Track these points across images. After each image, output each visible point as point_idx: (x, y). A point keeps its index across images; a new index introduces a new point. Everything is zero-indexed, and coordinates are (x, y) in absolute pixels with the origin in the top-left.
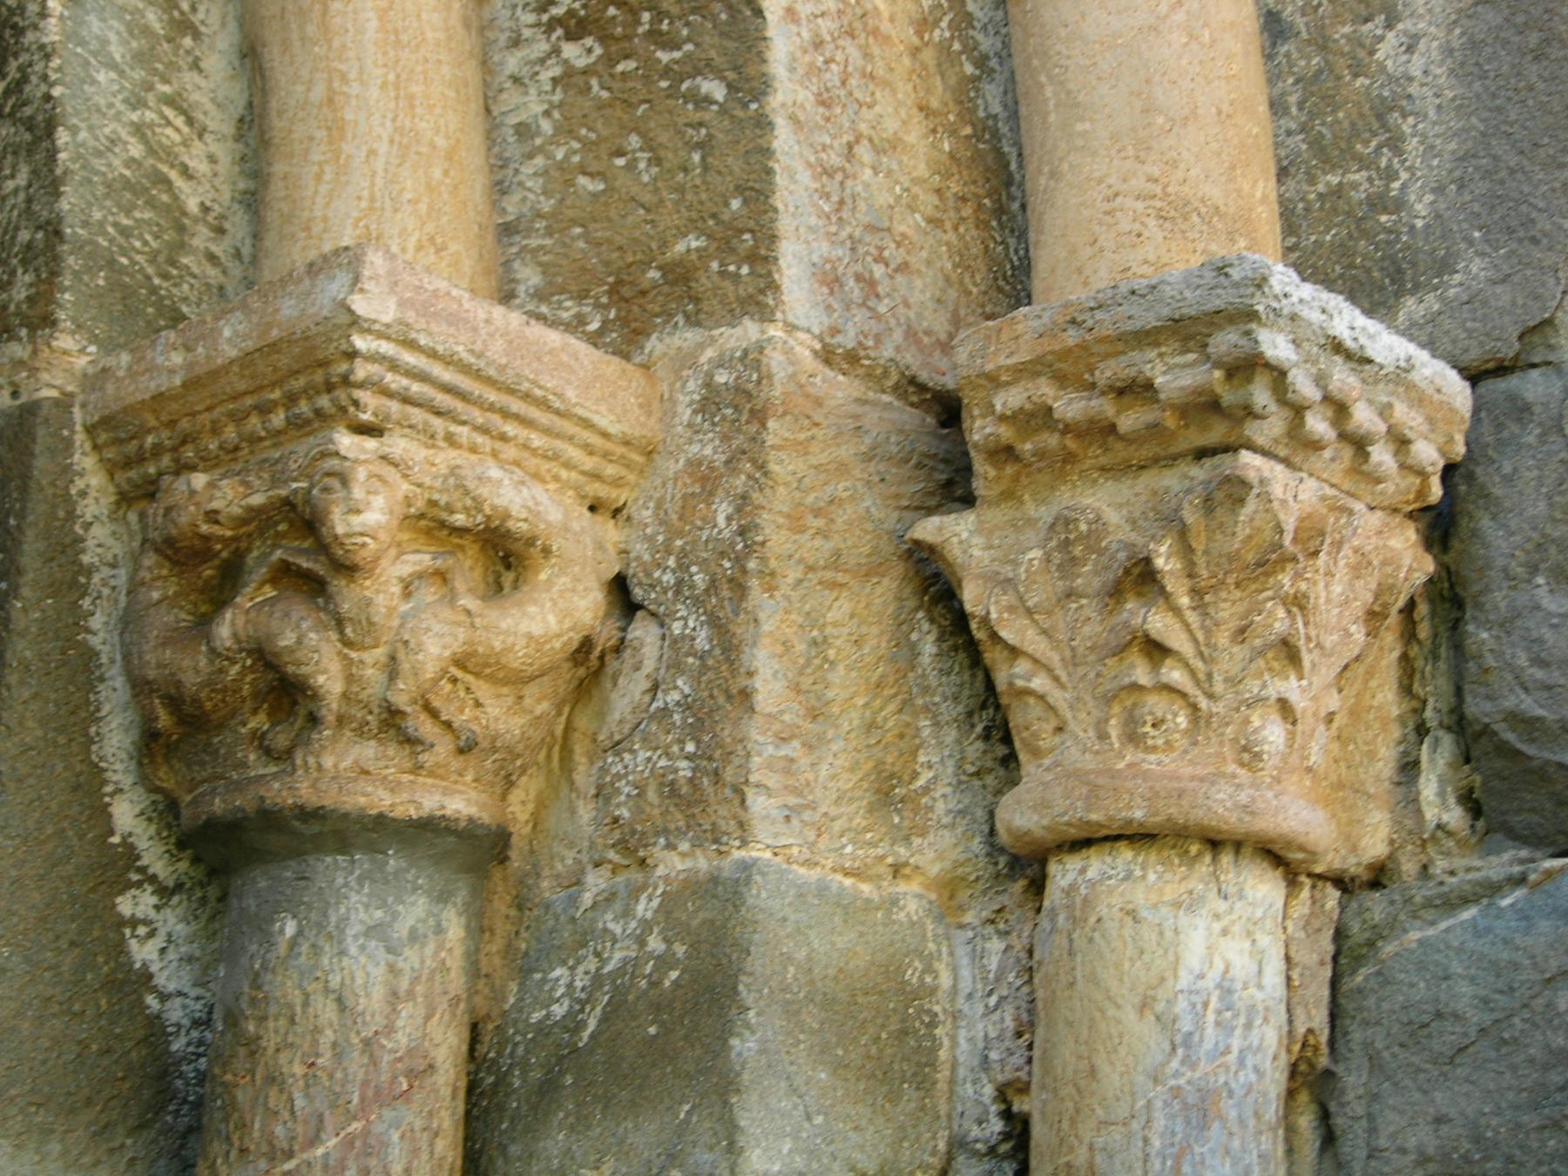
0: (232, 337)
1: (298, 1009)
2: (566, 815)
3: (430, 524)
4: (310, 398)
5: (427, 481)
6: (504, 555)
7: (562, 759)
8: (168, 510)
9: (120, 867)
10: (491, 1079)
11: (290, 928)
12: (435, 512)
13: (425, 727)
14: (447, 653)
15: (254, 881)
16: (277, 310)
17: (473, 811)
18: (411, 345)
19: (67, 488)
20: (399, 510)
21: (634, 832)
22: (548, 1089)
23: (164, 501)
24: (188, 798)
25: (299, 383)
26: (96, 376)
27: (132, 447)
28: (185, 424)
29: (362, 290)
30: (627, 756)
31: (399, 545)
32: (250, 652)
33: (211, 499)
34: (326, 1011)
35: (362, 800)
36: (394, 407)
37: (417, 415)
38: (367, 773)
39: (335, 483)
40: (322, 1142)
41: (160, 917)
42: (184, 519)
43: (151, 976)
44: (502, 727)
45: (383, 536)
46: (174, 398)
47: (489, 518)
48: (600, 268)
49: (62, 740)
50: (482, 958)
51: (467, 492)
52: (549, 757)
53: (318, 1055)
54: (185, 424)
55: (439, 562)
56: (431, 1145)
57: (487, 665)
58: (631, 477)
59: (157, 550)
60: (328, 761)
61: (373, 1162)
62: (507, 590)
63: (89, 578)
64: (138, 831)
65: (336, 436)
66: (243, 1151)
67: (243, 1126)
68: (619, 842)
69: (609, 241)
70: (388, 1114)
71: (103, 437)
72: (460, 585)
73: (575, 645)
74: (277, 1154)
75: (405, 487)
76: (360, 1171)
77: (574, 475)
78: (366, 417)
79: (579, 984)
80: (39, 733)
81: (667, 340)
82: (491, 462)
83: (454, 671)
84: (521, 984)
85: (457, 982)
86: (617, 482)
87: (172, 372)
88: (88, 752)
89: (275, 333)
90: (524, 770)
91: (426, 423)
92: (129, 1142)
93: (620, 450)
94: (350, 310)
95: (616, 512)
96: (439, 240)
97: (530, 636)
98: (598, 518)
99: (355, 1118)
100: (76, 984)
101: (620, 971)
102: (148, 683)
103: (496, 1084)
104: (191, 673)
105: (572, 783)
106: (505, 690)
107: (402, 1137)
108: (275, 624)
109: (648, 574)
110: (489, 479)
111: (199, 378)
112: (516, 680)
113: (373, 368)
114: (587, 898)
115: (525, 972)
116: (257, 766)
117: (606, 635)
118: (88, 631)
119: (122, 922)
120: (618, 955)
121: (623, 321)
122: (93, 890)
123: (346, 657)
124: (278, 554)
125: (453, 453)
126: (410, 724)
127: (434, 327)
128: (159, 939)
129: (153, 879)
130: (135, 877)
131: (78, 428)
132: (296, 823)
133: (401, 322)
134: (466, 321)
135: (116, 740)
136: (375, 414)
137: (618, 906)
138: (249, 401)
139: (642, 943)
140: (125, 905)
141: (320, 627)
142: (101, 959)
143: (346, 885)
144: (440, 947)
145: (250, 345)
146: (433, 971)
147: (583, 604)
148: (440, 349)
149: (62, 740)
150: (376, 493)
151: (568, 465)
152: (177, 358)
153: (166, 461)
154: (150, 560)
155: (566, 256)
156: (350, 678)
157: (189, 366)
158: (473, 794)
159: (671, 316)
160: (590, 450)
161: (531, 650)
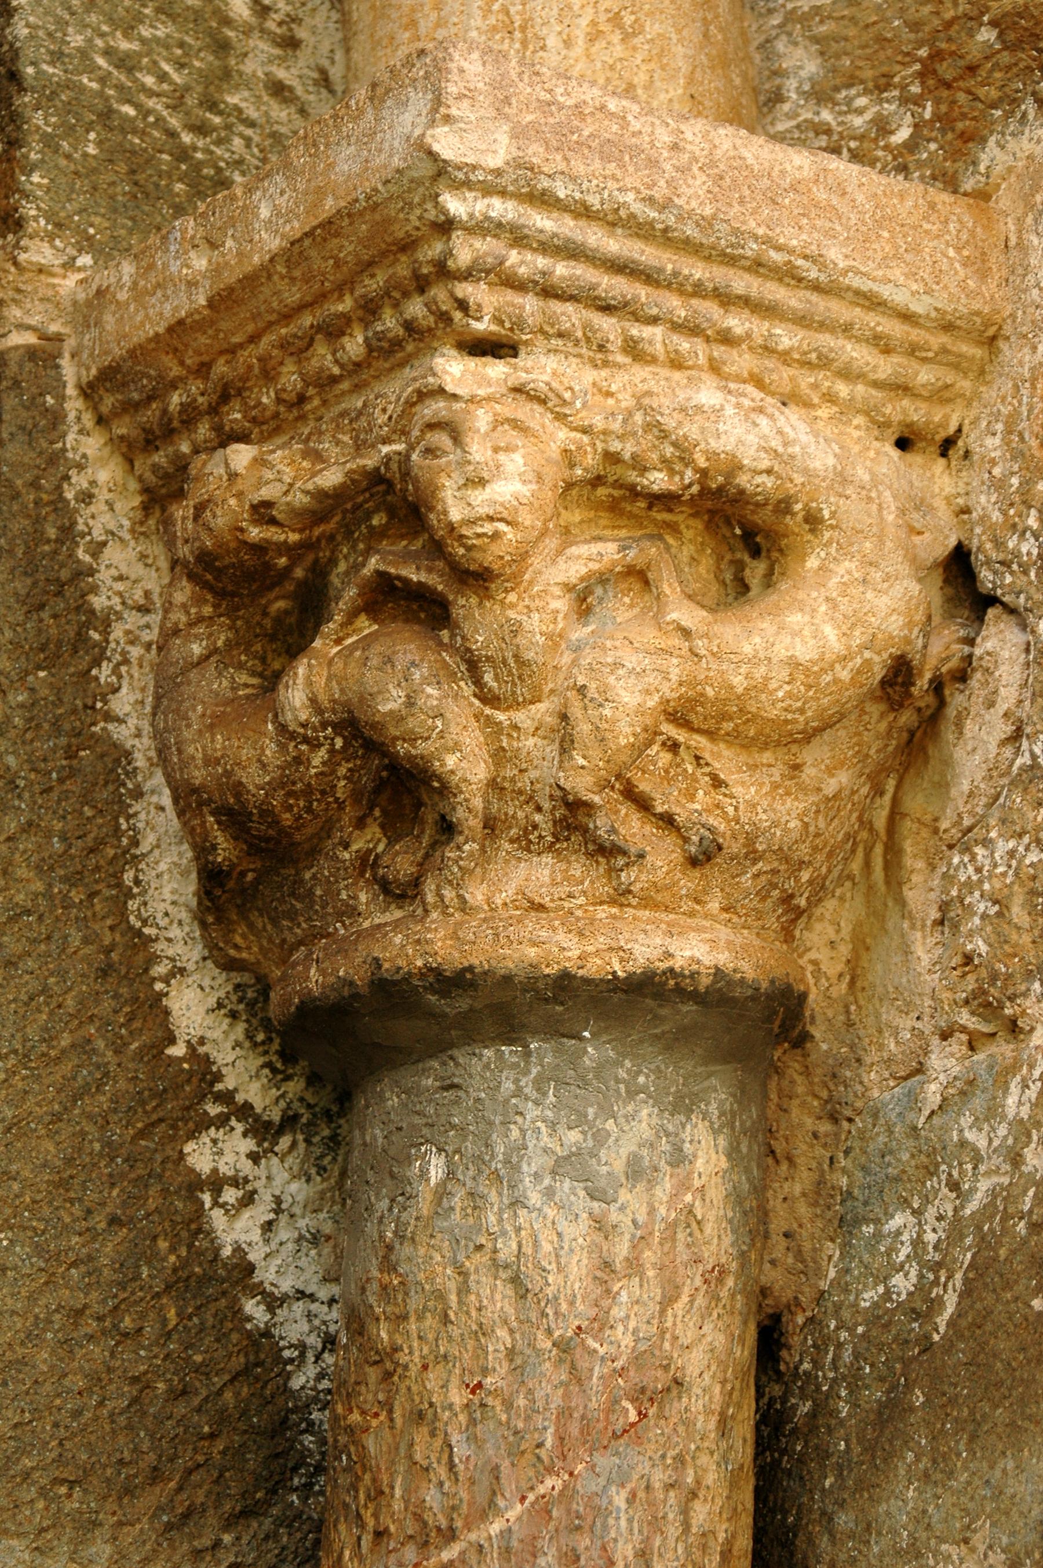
0: (270, 217)
1: (453, 1298)
2: (897, 959)
3: (610, 492)
4: (396, 305)
5: (598, 422)
6: (744, 534)
7: (887, 866)
8: (200, 509)
9: (190, 1094)
10: (806, 1407)
11: (436, 1168)
12: (615, 472)
13: (632, 828)
15: (383, 1099)
16: (331, 166)
17: (723, 958)
18: (544, 200)
19: (59, 488)
20: (555, 475)
21: (994, 977)
22: (890, 1413)
23: (197, 493)
25: (373, 284)
26: (89, 303)
27: (150, 414)
28: (221, 368)
29: (448, 119)
30: (979, 851)
31: (567, 531)
32: (338, 727)
33: (261, 483)
34: (496, 1299)
35: (532, 952)
36: (530, 304)
37: (570, 315)
38: (541, 908)
39: (442, 439)
40: (499, 1513)
41: (262, 1171)
42: (220, 521)
43: (251, 1269)
44: (763, 818)
45: (526, 518)
47: (704, 473)
48: (907, 35)
49: (77, 896)
50: (775, 1204)
51: (664, 435)
52: (867, 864)
53: (485, 1371)
54: (221, 368)
55: (632, 553)
56: (685, 1512)
57: (725, 717)
58: (965, 385)
59: (191, 577)
60: (476, 894)
61: (584, 1542)
63: (106, 633)
64: (217, 1034)
65: (439, 362)
66: (380, 1534)
67: (378, 1494)
68: (976, 994)
70: (604, 1461)
71: (108, 402)
72: (669, 587)
73: (879, 673)
74: (430, 1536)
75: (562, 435)
76: (562, 1556)
77: (860, 389)
78: (482, 326)
79: (930, 1237)
80: (39, 886)
81: (1012, 144)
82: (709, 381)
83: (670, 730)
84: (845, 1246)
85: (718, 1242)
86: (941, 395)
87: (192, 284)
88: (123, 914)
89: (330, 205)
90: (819, 890)
91: (587, 326)
92: (227, 1538)
93: (937, 340)
94: (430, 153)
95: (947, 446)
96: (628, 19)
97: (793, 664)
98: (916, 459)
99: (550, 1470)
100: (122, 1286)
101: (988, 1210)
102: (195, 791)
103: (813, 1415)
104: (253, 769)
105: (902, 902)
106: (767, 757)
107: (631, 1500)
109: (999, 544)
110: (699, 409)
111: (231, 290)
112: (781, 739)
113: (485, 246)
114: (933, 1093)
115: (846, 1226)
116: (375, 913)
117: (941, 648)
118: (109, 717)
119: (195, 1184)
120: (984, 1185)
121: (945, 120)
122: (142, 1134)
123: (489, 721)
124: (373, 563)
125: (640, 373)
126: (601, 824)
127: (579, 167)
128: (257, 1211)
129: (245, 1111)
131: (71, 391)
132: (433, 998)
133: (518, 164)
134: (636, 151)
135: (166, 888)
136: (498, 320)
137: (978, 1102)
138: (307, 320)
139: (1016, 1160)
140: (200, 1156)
141: (443, 676)
142: (163, 1245)
143: (518, 1093)
144: (684, 1186)
145: (296, 228)
146: (672, 1227)
147: (883, 603)
148: (594, 201)
149: (77, 896)
150: (509, 449)
151: (847, 374)
152: (200, 262)
156: (499, 756)
157: (216, 271)
158: (724, 933)
159: (1015, 102)
160: (883, 345)
161: (799, 687)
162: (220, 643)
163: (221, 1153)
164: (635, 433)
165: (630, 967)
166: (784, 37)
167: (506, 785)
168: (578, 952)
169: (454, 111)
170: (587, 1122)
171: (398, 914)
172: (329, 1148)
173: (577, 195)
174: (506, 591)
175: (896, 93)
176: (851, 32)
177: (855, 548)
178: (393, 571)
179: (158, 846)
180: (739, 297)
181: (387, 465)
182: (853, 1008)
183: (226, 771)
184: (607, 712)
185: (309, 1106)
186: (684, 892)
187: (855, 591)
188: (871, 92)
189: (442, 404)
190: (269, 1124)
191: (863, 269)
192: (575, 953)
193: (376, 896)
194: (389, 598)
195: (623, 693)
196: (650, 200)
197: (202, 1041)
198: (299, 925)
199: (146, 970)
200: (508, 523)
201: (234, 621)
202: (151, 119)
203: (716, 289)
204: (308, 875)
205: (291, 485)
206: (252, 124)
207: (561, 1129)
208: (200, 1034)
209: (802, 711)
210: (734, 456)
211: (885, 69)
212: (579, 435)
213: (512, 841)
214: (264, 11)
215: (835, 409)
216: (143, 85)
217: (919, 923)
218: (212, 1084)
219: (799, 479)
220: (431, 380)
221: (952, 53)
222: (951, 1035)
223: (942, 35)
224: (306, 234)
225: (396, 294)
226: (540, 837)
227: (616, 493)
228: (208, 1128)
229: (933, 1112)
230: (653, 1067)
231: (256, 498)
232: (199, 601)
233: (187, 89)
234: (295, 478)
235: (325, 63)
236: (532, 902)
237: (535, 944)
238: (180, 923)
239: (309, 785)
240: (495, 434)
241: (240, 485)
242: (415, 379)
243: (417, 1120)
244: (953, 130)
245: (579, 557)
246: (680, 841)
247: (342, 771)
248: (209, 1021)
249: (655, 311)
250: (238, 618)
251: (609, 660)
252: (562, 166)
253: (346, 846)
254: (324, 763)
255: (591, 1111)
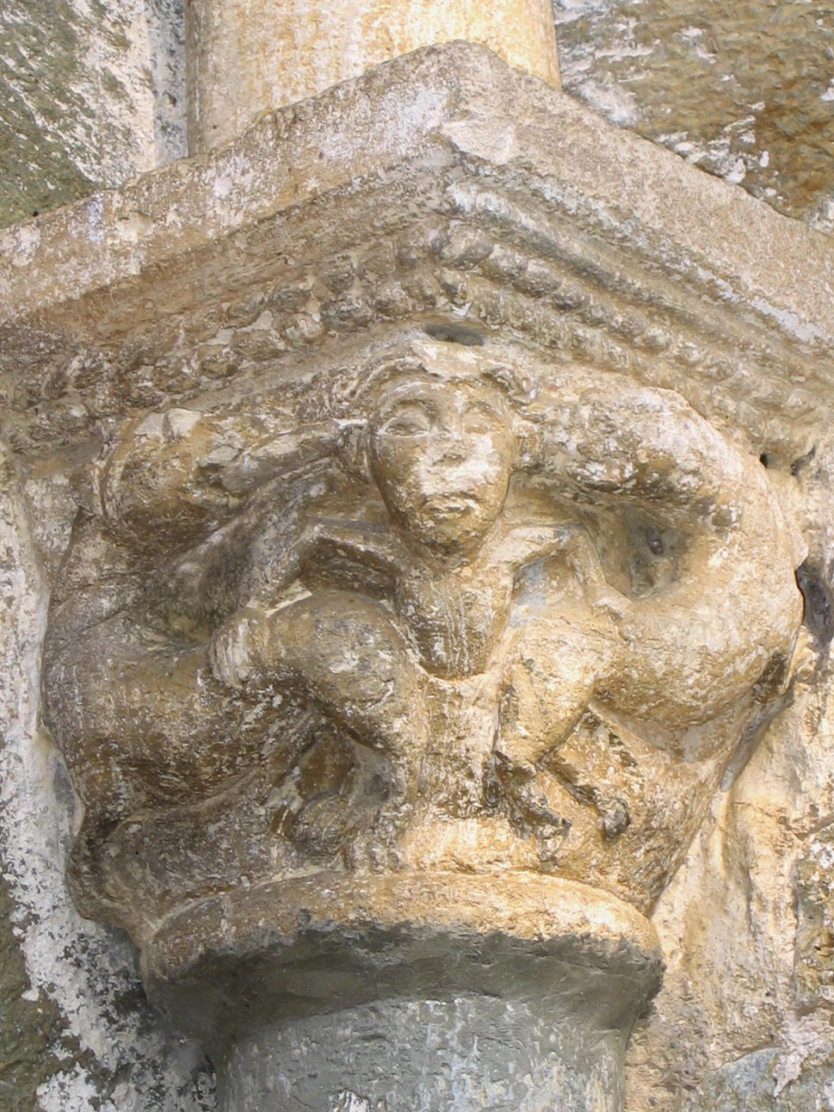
3: (534, 482)
8: (132, 468)
13: (554, 797)
14: (589, 680)
24: (156, 925)
29: (466, 114)
32: (279, 686)
33: (210, 447)
36: (504, 297)
37: (537, 311)
38: (469, 869)
39: (417, 416)
42: (162, 481)
45: (492, 496)
46: (124, 295)
47: (642, 468)
62: (659, 584)
64: (63, 982)
69: (750, 47)
87: (121, 253)
97: (704, 652)
108: (322, 644)
110: (643, 408)
111: (173, 260)
114: (791, 1066)
116: (284, 868)
123: (433, 689)
129: (87, 1058)
130: (62, 1055)
132: (361, 952)
134: (605, 163)
141: (395, 644)
143: (444, 1045)
148: (571, 205)
150: (481, 430)
151: (738, 391)
153: (103, 396)
154: (94, 549)
155: (675, 72)
156: (439, 722)
162: (129, 600)
163: (67, 1097)
164: (583, 426)
165: (553, 930)
166: (592, 84)
167: (442, 750)
168: (509, 914)
169: (470, 107)
170: (508, 1076)
171: (315, 870)
172: (156, 1098)
173: (559, 198)
174: (462, 565)
175: (727, 141)
176: (674, 83)
177: (755, 550)
178: (338, 539)
179: (16, 796)
180: (667, 309)
181: (346, 439)
182: (690, 983)
183: (143, 722)
184: (551, 686)
185: (139, 1057)
186: (594, 862)
187: (756, 589)
188: (697, 140)
189: (418, 383)
190: (105, 1072)
191: (768, 294)
192: (506, 914)
193: (287, 851)
194: (321, 566)
195: (563, 668)
196: (616, 209)
197: (52, 987)
198: (192, 877)
199: (7, 915)
200: (477, 500)
201: (144, 580)
202: (12, 100)
203: (650, 299)
204: (212, 829)
205: (241, 451)
206: (91, 115)
207: (486, 1081)
208: (50, 980)
209: (705, 699)
210: (671, 455)
211: (714, 118)
212: (529, 424)
213: (440, 805)
214: (101, 10)
215: (723, 422)
216: (6, 66)
217: (770, 907)
218: (60, 1031)
219: (716, 483)
220: (409, 359)
221: (793, 110)
222: (812, 1010)
223: (781, 92)
224: (280, 213)
225: (371, 277)
226: (469, 802)
227: (549, 482)
228: (57, 1073)
229: (791, 1083)
230: (561, 1026)
231: (206, 460)
232: (113, 558)
233: (41, 75)
234: (246, 445)
235: (149, 65)
236: (461, 864)
237: (469, 903)
238: (34, 872)
239: (238, 740)
240: (468, 416)
241: (184, 448)
242: (388, 358)
243: (333, 1068)
244: (795, 179)
245: (524, 539)
246: (594, 814)
247: (274, 729)
248: (58, 968)
249: (600, 314)
250: (149, 577)
251: (554, 638)
252: (553, 170)
253: (263, 802)
254: (257, 720)
255: (511, 1066)
